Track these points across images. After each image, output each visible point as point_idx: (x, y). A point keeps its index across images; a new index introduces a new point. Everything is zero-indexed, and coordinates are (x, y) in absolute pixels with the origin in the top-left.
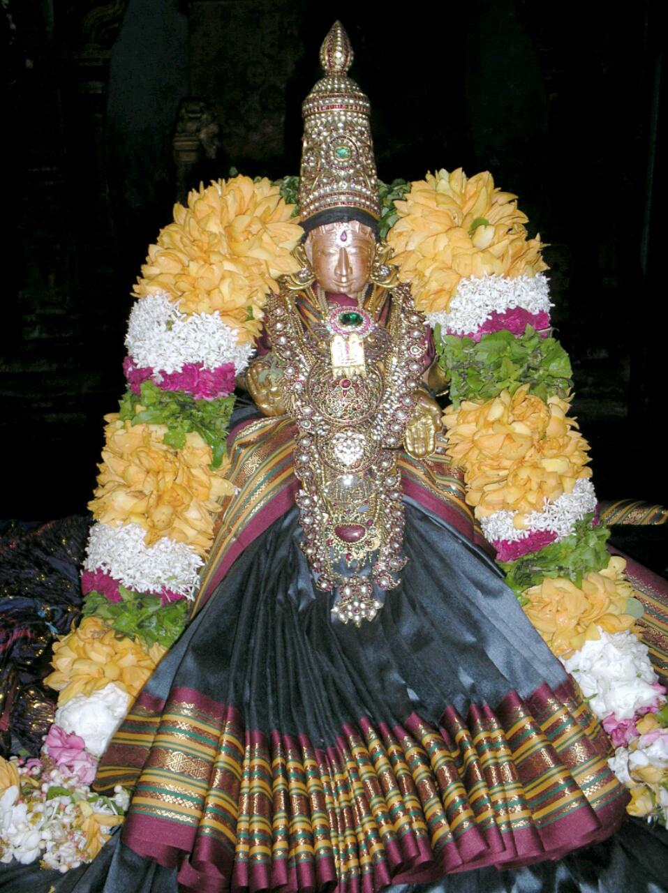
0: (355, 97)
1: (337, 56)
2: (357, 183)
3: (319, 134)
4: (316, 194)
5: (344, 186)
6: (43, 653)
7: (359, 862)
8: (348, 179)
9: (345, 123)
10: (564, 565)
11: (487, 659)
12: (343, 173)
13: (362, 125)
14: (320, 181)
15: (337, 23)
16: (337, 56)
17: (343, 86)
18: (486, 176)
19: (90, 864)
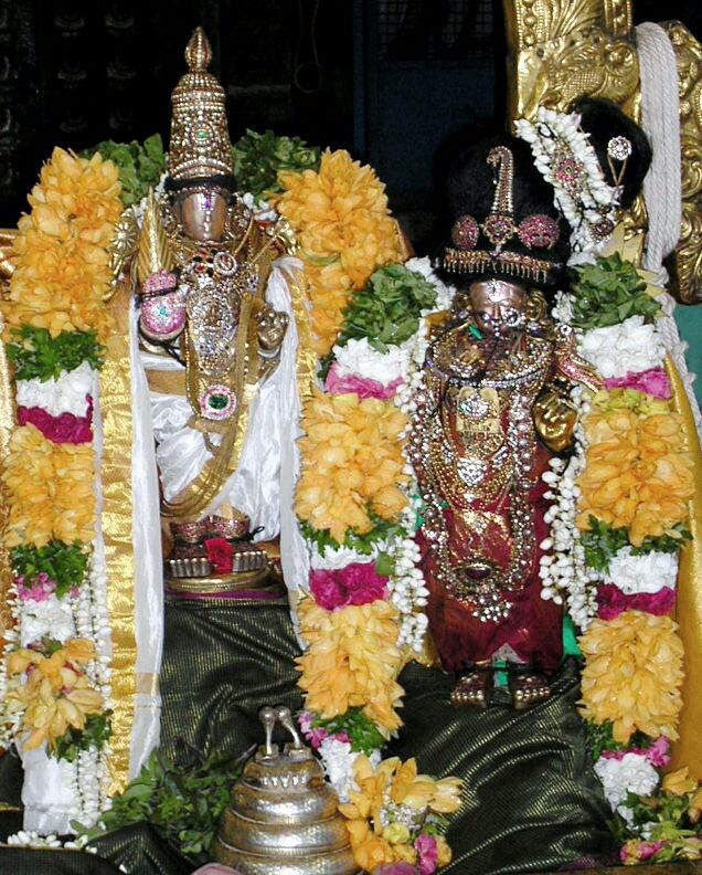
0: (212, 90)
1: (198, 54)
2: (215, 157)
3: (184, 119)
4: (181, 166)
5: (202, 159)
6: (91, 854)
7: (356, 819)
8: (206, 155)
9: (204, 111)
10: (11, 320)
11: (289, 616)
12: (202, 150)
13: (219, 112)
14: (185, 156)
15: (198, 29)
16: (198, 54)
17: (202, 81)
18: (384, 185)
19: (473, 216)
